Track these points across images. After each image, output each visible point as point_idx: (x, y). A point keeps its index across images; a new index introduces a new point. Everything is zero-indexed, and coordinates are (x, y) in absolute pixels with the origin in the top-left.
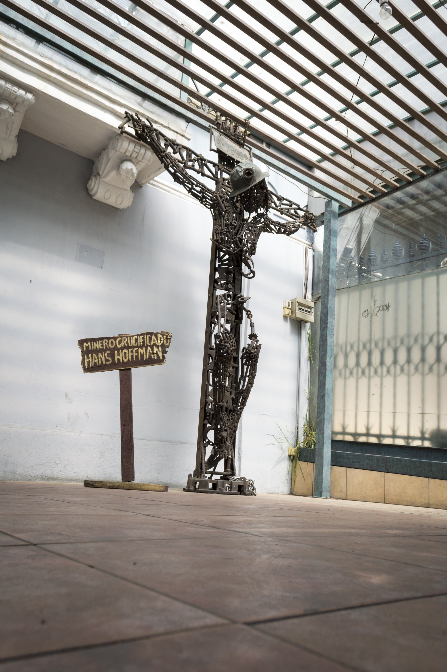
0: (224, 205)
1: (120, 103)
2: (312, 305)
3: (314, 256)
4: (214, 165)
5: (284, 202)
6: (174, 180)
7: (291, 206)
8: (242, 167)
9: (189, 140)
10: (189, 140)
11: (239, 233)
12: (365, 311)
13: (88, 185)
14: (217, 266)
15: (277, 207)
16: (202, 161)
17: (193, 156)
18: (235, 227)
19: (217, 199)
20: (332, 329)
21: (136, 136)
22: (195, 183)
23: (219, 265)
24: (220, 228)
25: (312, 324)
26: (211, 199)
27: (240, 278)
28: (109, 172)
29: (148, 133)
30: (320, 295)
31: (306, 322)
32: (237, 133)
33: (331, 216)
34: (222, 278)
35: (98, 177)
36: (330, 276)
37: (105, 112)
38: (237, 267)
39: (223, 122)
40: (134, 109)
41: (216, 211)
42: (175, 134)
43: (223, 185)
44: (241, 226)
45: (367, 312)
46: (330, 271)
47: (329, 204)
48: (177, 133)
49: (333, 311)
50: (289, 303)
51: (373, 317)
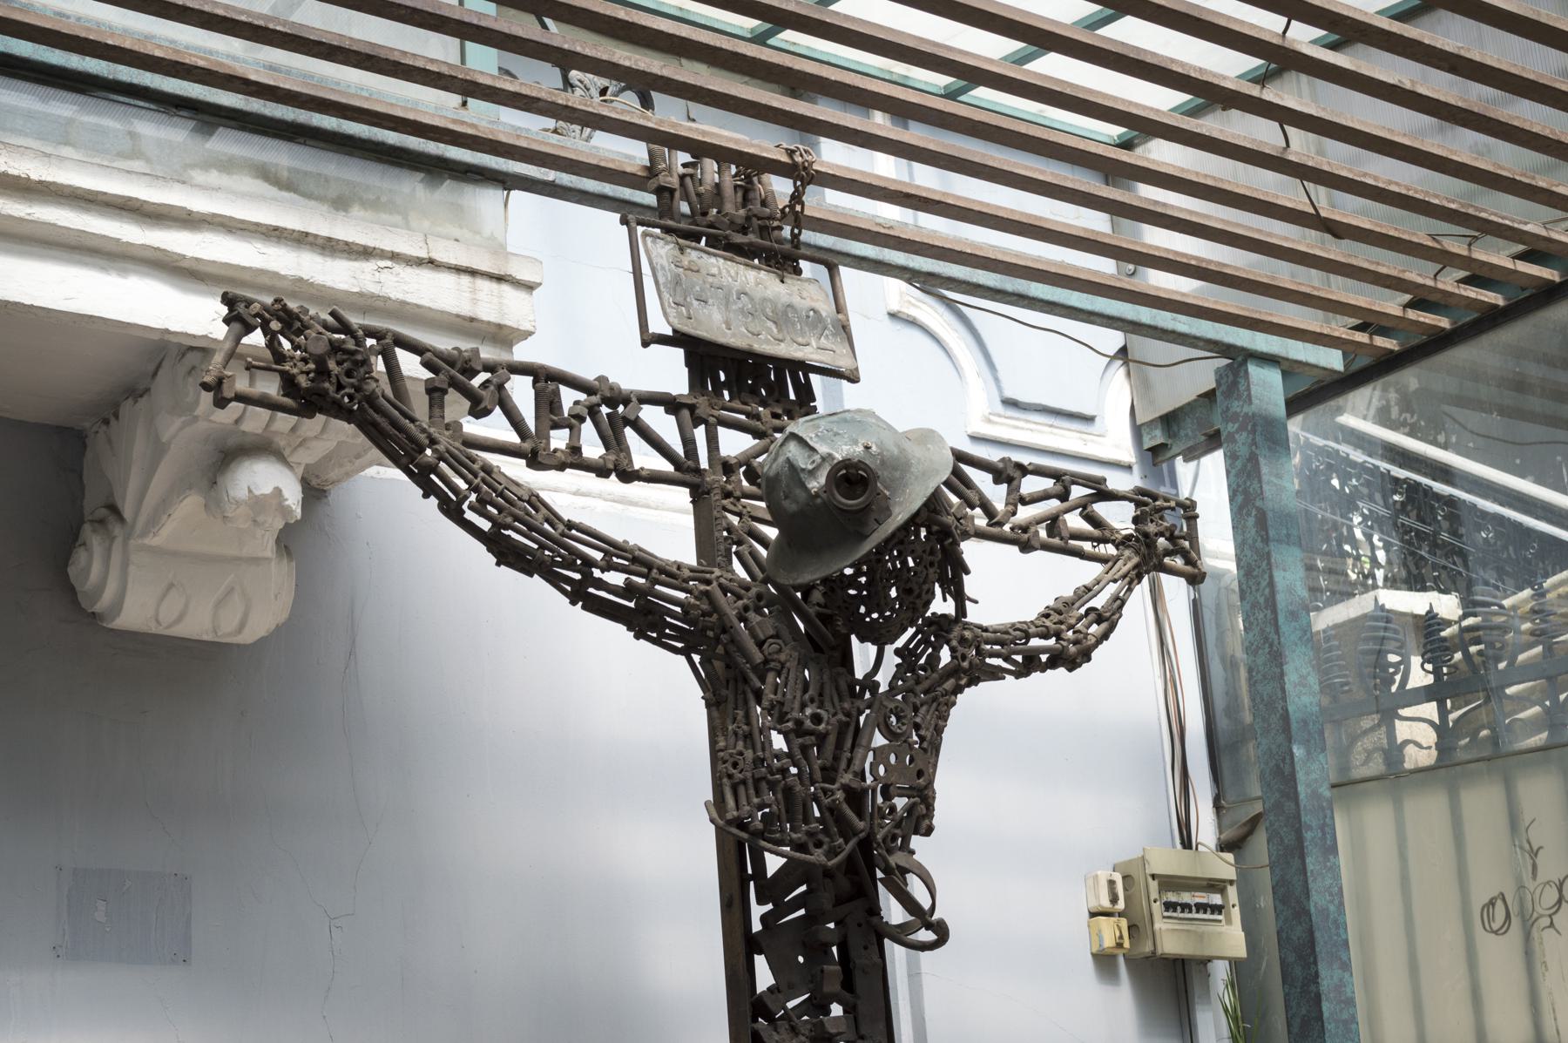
0: (753, 635)
1: (190, 213)
2: (1224, 866)
3: (1196, 608)
4: (671, 404)
5: (1030, 485)
6: (495, 560)
7: (1064, 497)
8: (813, 449)
9: (530, 287)
10: (530, 287)
11: (843, 765)
12: (1492, 903)
13: (72, 571)
14: (757, 926)
15: (1000, 524)
16: (613, 408)
17: (569, 398)
18: (822, 738)
19: (715, 608)
20: (1345, 1022)
21: (288, 401)
22: (598, 556)
23: (763, 918)
24: (749, 754)
25: (1235, 964)
26: (686, 612)
27: (876, 958)
28: (164, 506)
29: (345, 380)
30: (1258, 808)
31: (1204, 962)
32: (756, 207)
33: (1254, 443)
34: (791, 986)
35: (117, 530)
36: (1298, 751)
37: (123, 272)
38: (850, 899)
39: (682, 177)
40: (257, 224)
41: (717, 664)
42: (465, 280)
43: (728, 495)
44: (847, 724)
45: (1499, 903)
46: (1294, 726)
47: (1235, 384)
48: (473, 273)
49: (1340, 925)
50: (1111, 883)
51: (1535, 933)
